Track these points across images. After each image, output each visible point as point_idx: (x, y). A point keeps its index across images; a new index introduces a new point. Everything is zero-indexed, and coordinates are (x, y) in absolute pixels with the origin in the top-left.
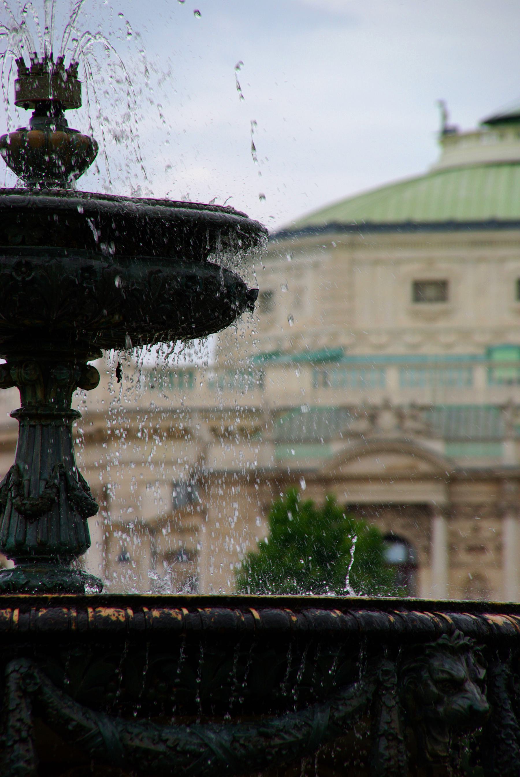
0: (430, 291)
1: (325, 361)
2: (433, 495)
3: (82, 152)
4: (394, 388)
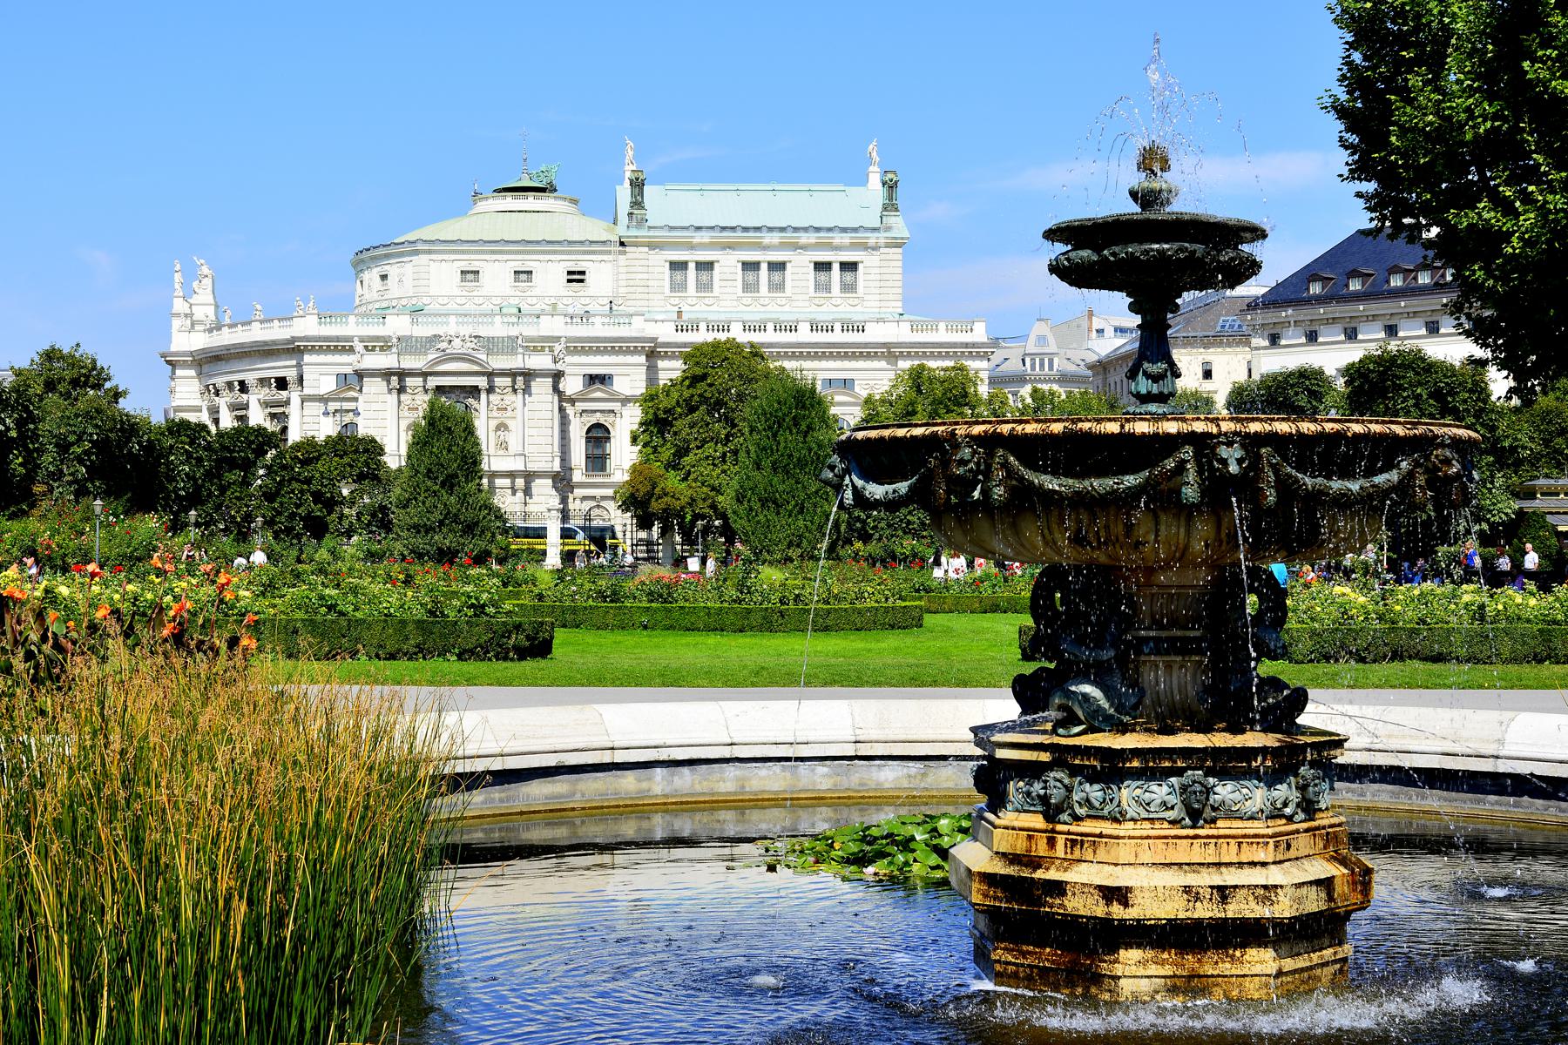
0: (470, 274)
1: (416, 312)
2: (482, 382)
4: (451, 327)
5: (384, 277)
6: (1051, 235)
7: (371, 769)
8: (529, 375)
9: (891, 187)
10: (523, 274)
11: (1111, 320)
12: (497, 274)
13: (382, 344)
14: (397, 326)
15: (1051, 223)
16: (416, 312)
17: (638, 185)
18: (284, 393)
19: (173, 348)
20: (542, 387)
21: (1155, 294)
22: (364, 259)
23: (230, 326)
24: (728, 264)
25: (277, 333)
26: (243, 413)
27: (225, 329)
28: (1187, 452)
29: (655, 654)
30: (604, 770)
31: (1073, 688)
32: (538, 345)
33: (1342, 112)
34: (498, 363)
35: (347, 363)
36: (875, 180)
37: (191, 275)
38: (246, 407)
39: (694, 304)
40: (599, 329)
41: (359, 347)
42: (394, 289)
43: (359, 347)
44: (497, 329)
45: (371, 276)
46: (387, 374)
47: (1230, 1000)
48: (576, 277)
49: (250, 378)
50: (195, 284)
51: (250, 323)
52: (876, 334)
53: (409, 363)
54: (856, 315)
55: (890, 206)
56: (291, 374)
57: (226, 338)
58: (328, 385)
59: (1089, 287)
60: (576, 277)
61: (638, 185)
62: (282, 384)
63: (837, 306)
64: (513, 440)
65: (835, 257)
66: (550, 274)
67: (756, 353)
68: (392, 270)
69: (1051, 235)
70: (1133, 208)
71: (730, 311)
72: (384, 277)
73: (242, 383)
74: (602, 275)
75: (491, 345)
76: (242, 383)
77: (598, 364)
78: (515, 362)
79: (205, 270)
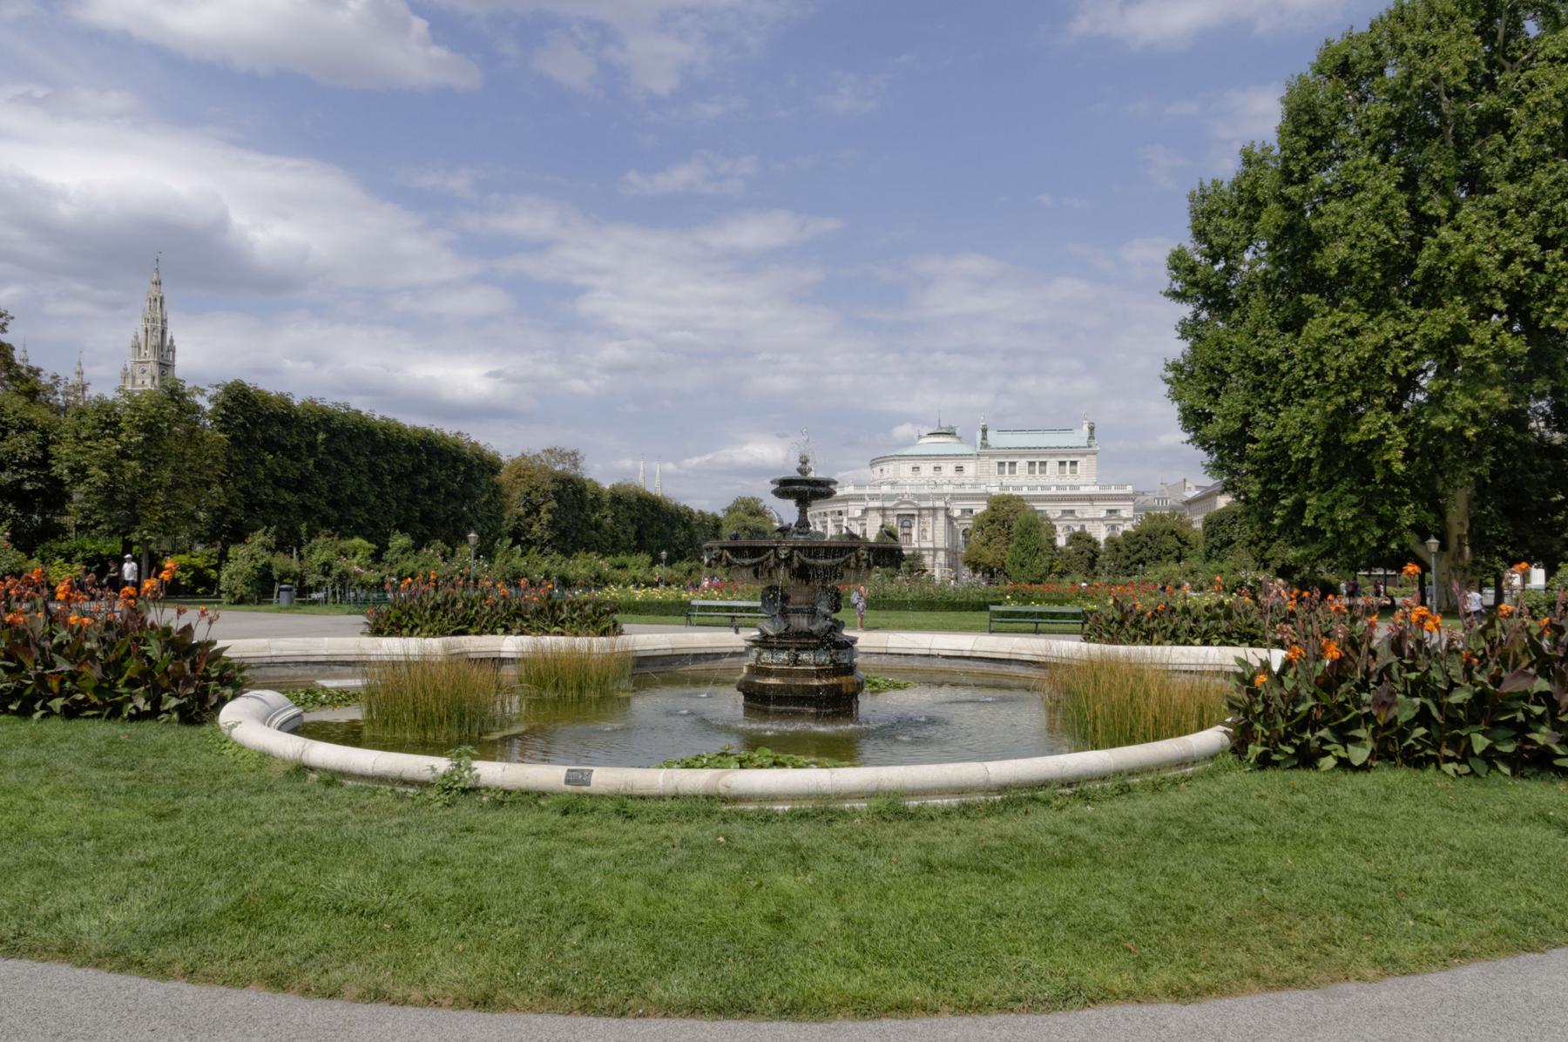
0: (916, 469)
1: (893, 484)
4: (908, 490)
8: (935, 509)
9: (1092, 429)
10: (937, 468)
12: (927, 469)
13: (873, 497)
14: (886, 489)
16: (893, 484)
17: (984, 431)
20: (941, 516)
21: (803, 501)
22: (873, 463)
24: (1022, 463)
30: (1017, 661)
31: (1355, 437)
32: (940, 497)
33: (1167, 381)
34: (923, 504)
35: (864, 505)
36: (1086, 428)
39: (1007, 479)
40: (968, 490)
42: (886, 475)
44: (926, 490)
45: (877, 469)
46: (878, 509)
47: (1332, 446)
48: (959, 469)
52: (1084, 490)
53: (888, 504)
54: (1076, 483)
55: (1091, 437)
58: (858, 513)
60: (959, 469)
61: (984, 431)
62: (840, 513)
63: (1069, 479)
64: (929, 536)
65: (1007, 460)
66: (948, 468)
67: (1020, 499)
68: (885, 467)
71: (1021, 483)
74: (970, 468)
75: (920, 497)
77: (1113, 505)
78: (930, 504)
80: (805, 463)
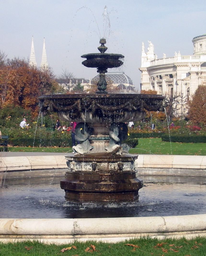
3: (106, 49)
5: (201, 45)
6: (82, 57)
7: (200, 207)
11: (93, 73)
15: (82, 55)
18: (172, 79)
19: (142, 66)
23: (157, 60)
25: (170, 61)
26: (160, 84)
27: (156, 61)
28: (79, 101)
29: (69, 155)
35: (187, 70)
37: (147, 46)
38: (161, 83)
41: (190, 65)
43: (190, 65)
49: (162, 75)
50: (148, 49)
51: (162, 59)
56: (173, 73)
57: (156, 63)
58: (184, 76)
59: (90, 67)
62: (171, 76)
69: (82, 57)
70: (99, 52)
72: (201, 45)
73: (160, 76)
76: (160, 76)
79: (151, 44)
80: (103, 44)
